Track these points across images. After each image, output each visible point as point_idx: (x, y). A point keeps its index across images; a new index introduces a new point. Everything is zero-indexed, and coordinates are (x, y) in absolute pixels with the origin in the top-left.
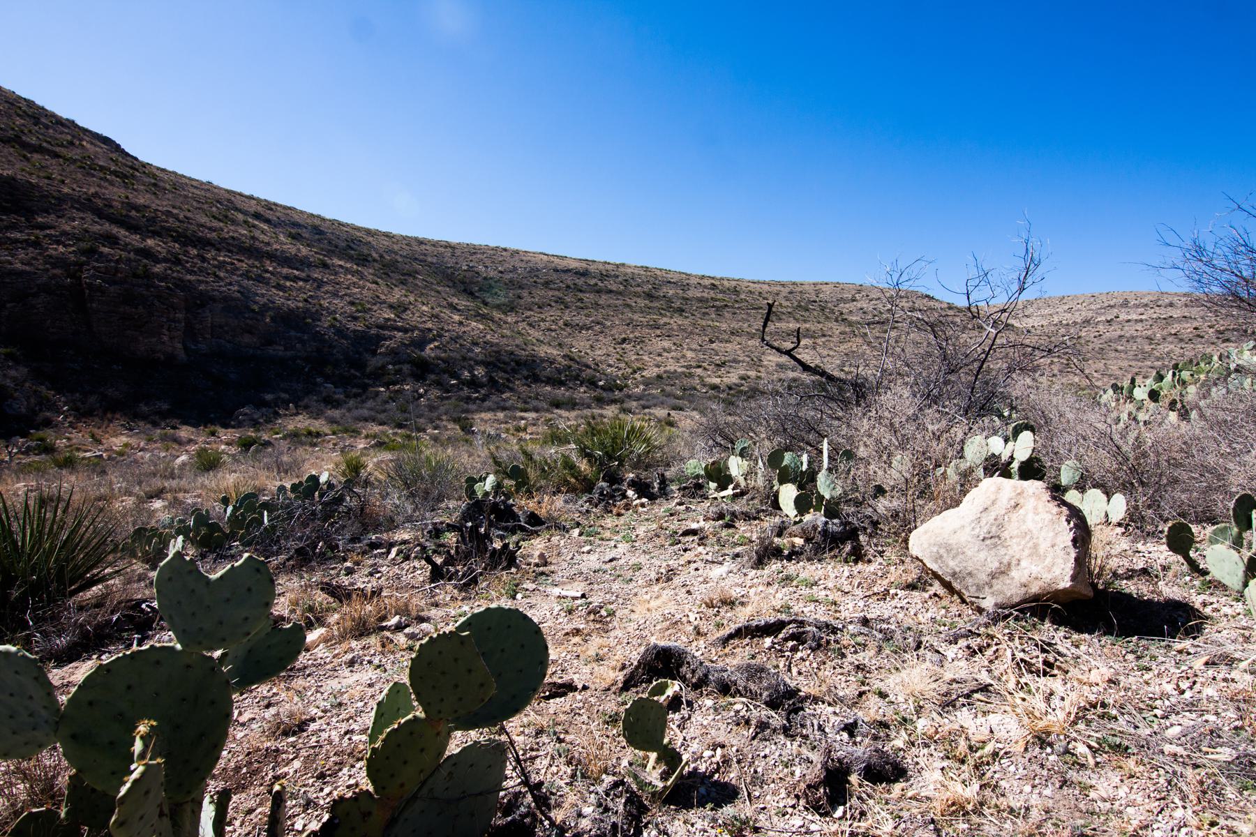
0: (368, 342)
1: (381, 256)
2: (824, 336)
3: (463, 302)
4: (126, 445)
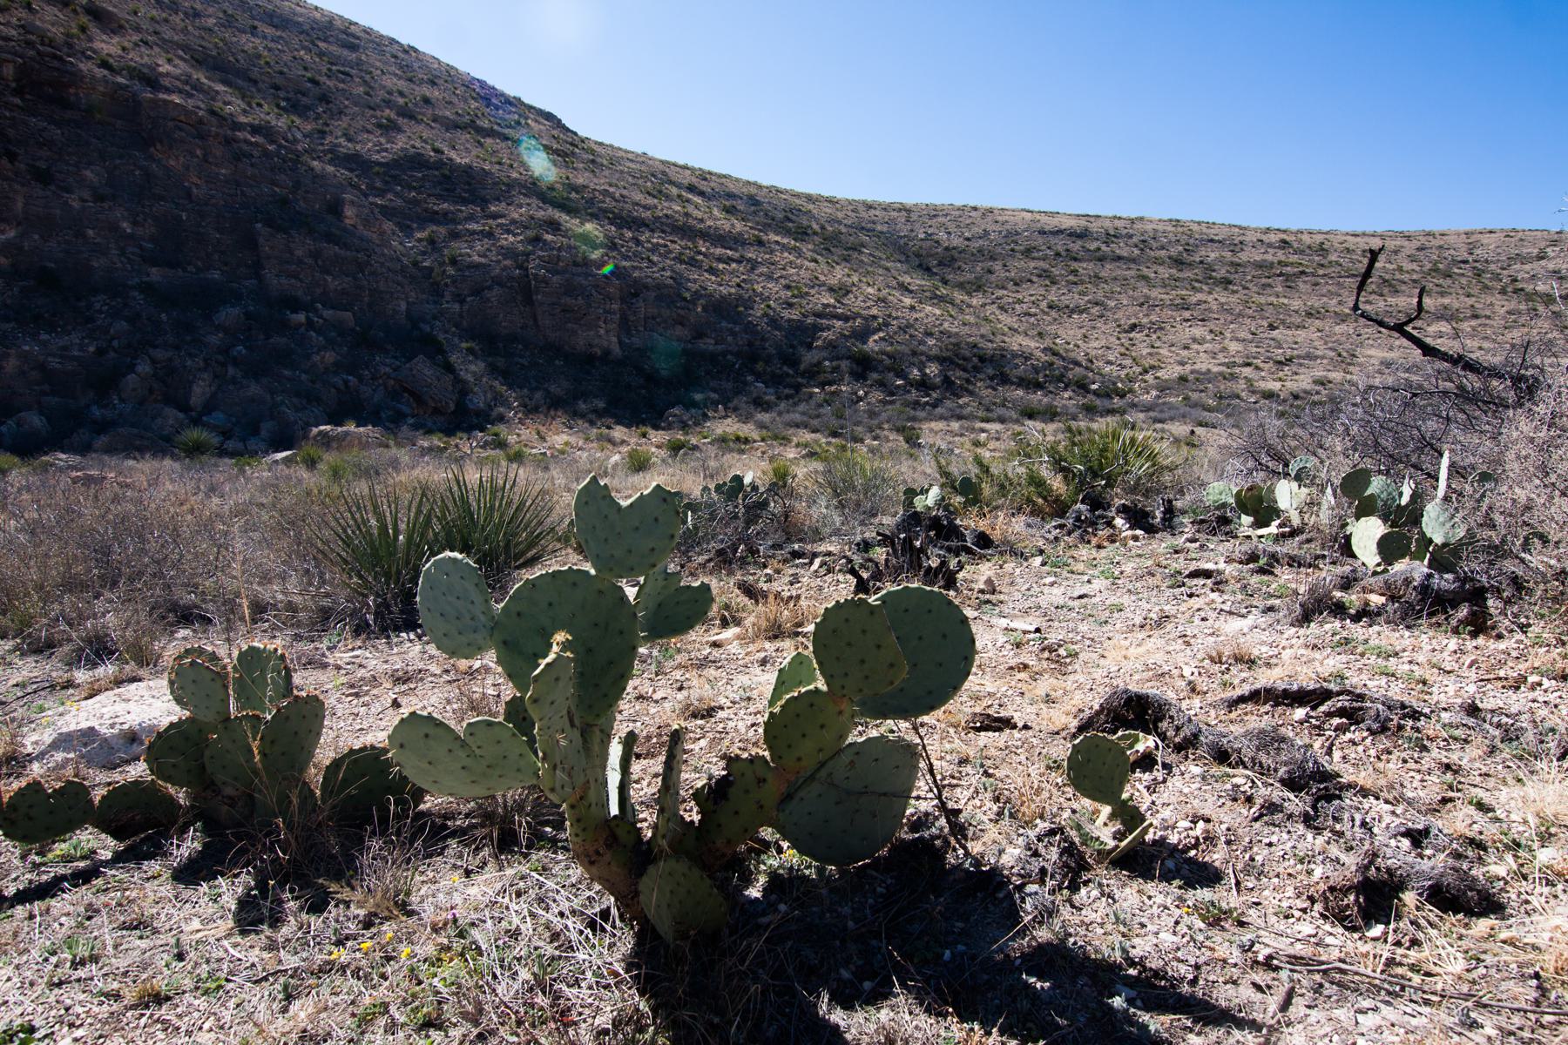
0: (803, 333)
1: (823, 228)
2: (1476, 317)
3: (916, 281)
4: (566, 444)
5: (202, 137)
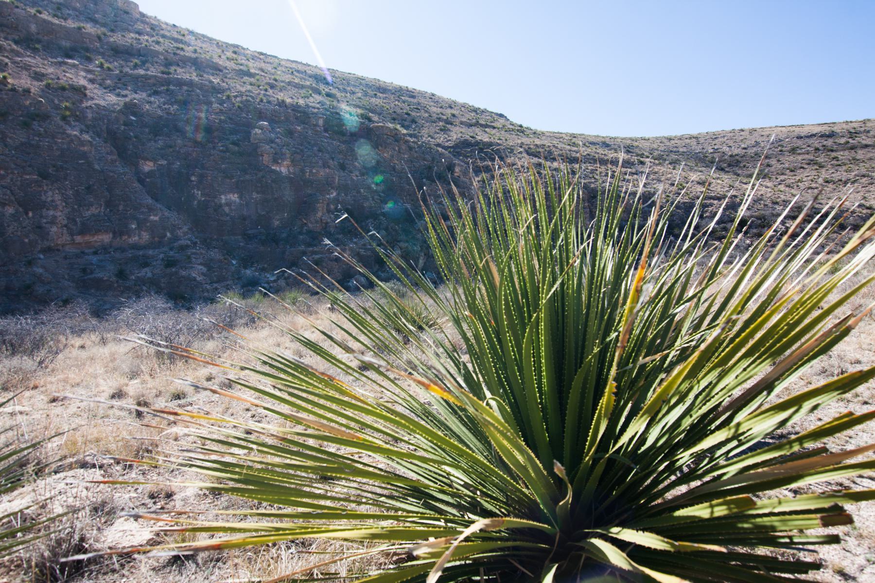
5: (397, 141)
